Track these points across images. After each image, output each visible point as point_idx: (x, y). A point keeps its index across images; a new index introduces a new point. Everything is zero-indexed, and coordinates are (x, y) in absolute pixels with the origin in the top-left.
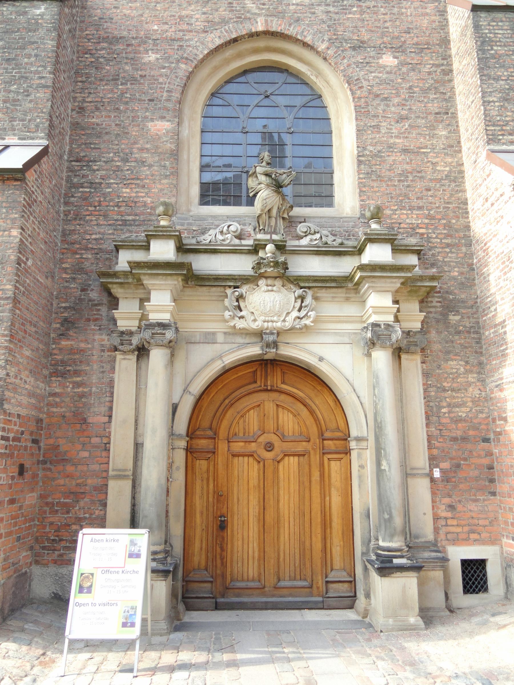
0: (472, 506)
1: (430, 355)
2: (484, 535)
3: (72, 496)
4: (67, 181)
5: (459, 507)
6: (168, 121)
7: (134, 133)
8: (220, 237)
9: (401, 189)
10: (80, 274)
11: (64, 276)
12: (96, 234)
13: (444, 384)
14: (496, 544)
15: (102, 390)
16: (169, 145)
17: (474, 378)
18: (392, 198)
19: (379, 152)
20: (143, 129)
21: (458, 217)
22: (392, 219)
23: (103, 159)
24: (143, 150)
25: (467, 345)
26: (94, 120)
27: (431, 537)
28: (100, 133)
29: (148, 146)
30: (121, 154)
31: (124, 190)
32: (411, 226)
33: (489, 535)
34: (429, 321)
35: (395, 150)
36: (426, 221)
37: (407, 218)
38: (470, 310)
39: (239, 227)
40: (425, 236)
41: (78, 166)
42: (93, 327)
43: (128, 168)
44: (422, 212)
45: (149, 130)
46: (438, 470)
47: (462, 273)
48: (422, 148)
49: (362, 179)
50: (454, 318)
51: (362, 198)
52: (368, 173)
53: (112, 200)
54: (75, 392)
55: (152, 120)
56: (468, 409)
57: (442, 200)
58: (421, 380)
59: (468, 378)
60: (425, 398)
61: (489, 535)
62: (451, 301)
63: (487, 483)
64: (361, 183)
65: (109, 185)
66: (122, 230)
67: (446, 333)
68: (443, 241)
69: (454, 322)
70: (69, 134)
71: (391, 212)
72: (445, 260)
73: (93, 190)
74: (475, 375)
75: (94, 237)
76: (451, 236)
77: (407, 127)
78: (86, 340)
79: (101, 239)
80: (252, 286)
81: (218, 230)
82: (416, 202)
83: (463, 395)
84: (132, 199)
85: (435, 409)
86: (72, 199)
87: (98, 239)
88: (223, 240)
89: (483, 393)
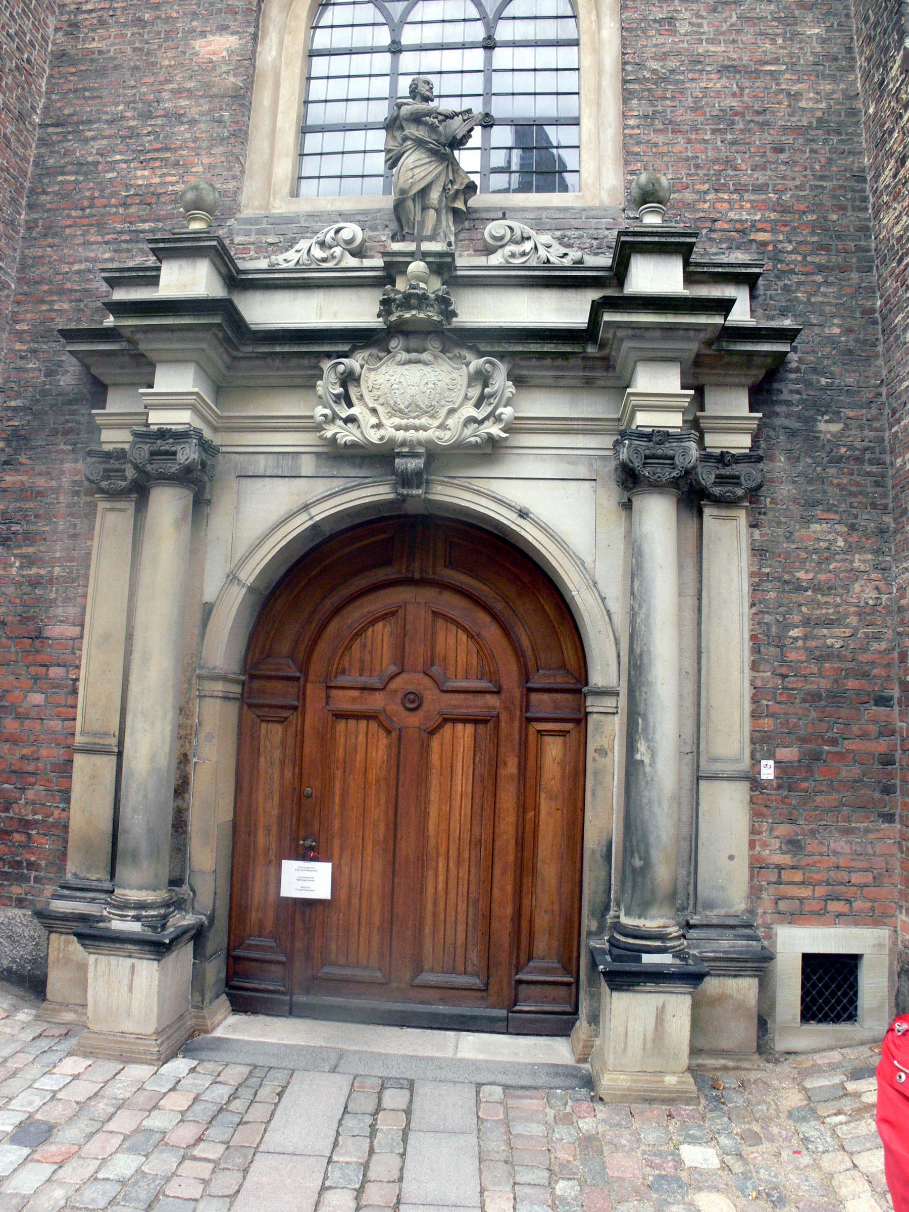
0: (840, 844)
1: (771, 509)
2: (858, 905)
3: (14, 778)
4: (36, 164)
5: (812, 845)
6: (232, 34)
7: (167, 63)
8: (318, 253)
9: (718, 149)
10: (46, 343)
11: (18, 346)
12: (81, 262)
13: (798, 574)
14: (885, 924)
15: (70, 573)
16: (232, 79)
17: (865, 561)
18: (697, 167)
19: (672, 71)
20: (184, 53)
21: (843, 208)
22: (698, 210)
23: (104, 117)
24: (180, 93)
25: (854, 489)
26: (94, 45)
27: (739, 904)
28: (104, 69)
29: (191, 84)
30: (140, 105)
31: (139, 173)
32: (738, 226)
33: (869, 905)
34: (772, 434)
35: (708, 69)
36: (773, 216)
37: (731, 209)
38: (864, 411)
39: (360, 236)
40: (770, 248)
41: (57, 134)
42: (62, 446)
43: (150, 129)
44: (764, 197)
45: (196, 54)
46: (771, 763)
47: (849, 331)
48: (766, 63)
49: (632, 128)
50: (828, 428)
51: (630, 168)
52: (646, 116)
53: (113, 194)
54: (23, 576)
55: (203, 34)
56: (848, 632)
57: (808, 172)
58: (744, 564)
59: (852, 562)
60: (753, 605)
61: (869, 905)
62: (824, 389)
63: (877, 795)
64: (631, 136)
65: (112, 166)
66: (128, 251)
67: (809, 460)
68: (809, 259)
69: (828, 436)
70: (46, 75)
71: (696, 197)
72: (813, 300)
73: (81, 178)
74: (870, 557)
75: (76, 267)
76: (826, 248)
77: (734, 19)
78: (49, 473)
79: (89, 271)
80: (374, 351)
81: (314, 240)
82: (751, 176)
83: (838, 600)
84: (152, 189)
85: (774, 629)
86: (43, 198)
87: (84, 271)
88: (324, 260)
89: (884, 597)
